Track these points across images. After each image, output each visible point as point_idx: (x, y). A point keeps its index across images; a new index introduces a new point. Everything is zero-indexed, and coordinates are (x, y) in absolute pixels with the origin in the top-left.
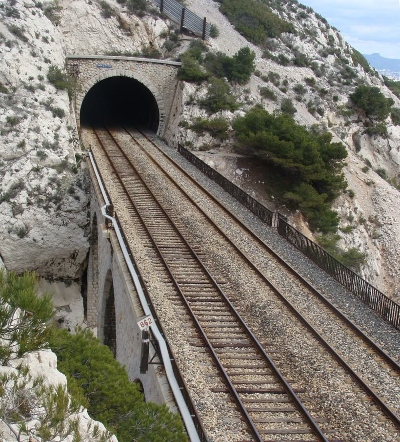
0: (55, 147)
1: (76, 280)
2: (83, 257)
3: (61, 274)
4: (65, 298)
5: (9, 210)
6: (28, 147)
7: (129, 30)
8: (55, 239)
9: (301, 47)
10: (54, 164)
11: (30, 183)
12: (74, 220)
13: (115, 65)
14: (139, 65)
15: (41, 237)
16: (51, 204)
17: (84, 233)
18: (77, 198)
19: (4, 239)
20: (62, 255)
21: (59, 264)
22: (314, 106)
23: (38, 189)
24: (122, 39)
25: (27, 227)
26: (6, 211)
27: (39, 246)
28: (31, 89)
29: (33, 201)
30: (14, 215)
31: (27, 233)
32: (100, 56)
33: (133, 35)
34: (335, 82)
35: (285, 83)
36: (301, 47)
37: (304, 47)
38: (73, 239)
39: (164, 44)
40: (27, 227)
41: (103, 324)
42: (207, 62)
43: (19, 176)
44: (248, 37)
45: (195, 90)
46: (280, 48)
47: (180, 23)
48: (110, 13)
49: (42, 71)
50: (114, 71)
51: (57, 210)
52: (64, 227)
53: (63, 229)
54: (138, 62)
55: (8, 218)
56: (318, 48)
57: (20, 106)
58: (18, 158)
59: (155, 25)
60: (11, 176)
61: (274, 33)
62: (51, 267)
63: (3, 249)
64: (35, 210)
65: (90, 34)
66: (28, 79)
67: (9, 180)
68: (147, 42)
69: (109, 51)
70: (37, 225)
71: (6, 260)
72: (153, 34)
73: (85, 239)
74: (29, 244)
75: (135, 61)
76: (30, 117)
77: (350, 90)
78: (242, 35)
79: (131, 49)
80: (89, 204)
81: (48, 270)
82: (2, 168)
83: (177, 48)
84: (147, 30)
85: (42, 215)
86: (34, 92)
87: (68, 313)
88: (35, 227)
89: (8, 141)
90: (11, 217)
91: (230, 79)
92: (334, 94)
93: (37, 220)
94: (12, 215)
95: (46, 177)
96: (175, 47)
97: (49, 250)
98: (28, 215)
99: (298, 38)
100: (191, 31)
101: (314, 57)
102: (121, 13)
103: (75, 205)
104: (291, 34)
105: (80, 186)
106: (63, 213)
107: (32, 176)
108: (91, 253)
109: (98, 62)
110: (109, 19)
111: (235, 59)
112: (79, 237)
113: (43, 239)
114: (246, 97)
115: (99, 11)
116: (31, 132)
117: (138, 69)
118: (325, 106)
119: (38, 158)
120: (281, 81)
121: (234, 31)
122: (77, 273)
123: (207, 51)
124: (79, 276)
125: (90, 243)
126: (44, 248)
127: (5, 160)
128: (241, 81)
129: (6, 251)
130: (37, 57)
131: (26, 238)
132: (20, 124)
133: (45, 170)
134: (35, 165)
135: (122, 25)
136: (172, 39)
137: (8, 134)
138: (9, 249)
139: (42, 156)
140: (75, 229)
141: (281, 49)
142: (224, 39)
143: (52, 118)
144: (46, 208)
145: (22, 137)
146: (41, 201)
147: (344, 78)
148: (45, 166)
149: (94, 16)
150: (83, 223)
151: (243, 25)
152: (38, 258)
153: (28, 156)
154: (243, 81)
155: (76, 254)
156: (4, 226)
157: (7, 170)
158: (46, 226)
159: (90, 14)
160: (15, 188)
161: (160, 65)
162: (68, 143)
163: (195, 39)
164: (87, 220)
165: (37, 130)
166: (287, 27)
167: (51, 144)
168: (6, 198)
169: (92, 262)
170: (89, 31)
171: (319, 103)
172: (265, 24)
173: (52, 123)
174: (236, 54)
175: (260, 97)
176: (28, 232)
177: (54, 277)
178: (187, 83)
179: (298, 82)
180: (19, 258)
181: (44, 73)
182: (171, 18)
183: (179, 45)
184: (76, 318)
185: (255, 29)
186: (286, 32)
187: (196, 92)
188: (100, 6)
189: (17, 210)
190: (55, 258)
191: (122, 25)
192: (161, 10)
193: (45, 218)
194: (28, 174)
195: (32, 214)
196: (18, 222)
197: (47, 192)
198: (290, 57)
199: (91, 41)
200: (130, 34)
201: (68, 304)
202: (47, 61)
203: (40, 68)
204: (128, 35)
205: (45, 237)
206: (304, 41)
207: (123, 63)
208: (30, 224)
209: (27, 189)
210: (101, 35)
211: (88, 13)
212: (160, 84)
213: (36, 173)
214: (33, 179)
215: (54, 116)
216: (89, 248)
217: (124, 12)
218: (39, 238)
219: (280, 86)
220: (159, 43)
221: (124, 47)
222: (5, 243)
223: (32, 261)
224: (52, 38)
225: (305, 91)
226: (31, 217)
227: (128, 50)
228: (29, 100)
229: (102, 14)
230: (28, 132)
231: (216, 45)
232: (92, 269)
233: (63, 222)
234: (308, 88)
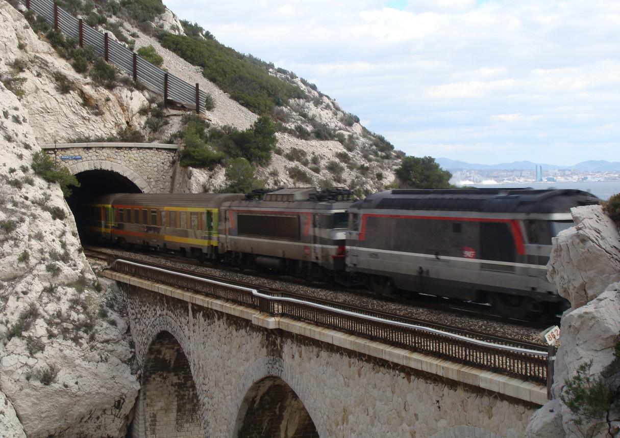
0: (65, 258)
2: (131, 404)
5: (23, 348)
6: (33, 261)
7: (97, 107)
8: (94, 382)
9: (318, 115)
10: (70, 281)
11: (46, 309)
12: (114, 353)
13: (86, 155)
17: (130, 370)
19: (21, 390)
20: (103, 404)
21: (98, 418)
22: (358, 187)
23: (59, 314)
24: (89, 120)
25: (52, 369)
26: (19, 350)
27: (73, 394)
28: (17, 184)
29: (56, 332)
30: (32, 354)
31: (54, 378)
32: (62, 144)
33: (104, 113)
34: (372, 156)
36: (318, 115)
37: (322, 115)
39: (147, 123)
40: (52, 369)
42: (213, 140)
43: (29, 300)
44: (251, 106)
45: (208, 178)
46: (293, 118)
48: (69, 87)
50: (86, 163)
52: (103, 364)
53: (103, 367)
54: (118, 148)
55: (24, 359)
56: (338, 115)
57: (10, 206)
58: (22, 277)
59: (131, 99)
60: (17, 301)
61: (282, 100)
62: (85, 425)
63: (21, 405)
65: (44, 117)
66: (7, 171)
67: (15, 308)
68: (124, 121)
70: (67, 365)
71: (25, 421)
72: (130, 111)
74: (57, 392)
75: (113, 147)
76: (27, 219)
77: (394, 165)
78: (242, 104)
79: (103, 133)
80: (129, 330)
81: (82, 430)
82: (2, 291)
83: (164, 127)
84: (121, 105)
85: (71, 350)
86: (20, 188)
88: (64, 369)
89: (6, 254)
90: (29, 357)
92: (376, 171)
93: (65, 357)
95: (64, 299)
96: (161, 126)
97: (87, 399)
98: (52, 352)
99: (311, 105)
100: (180, 103)
101: (336, 126)
102: (83, 86)
103: (113, 333)
105: (111, 307)
106: (99, 345)
107: (45, 300)
108: (141, 398)
109: (63, 152)
110: (68, 95)
111: (252, 132)
112: (125, 375)
113: (77, 383)
114: (275, 181)
115: (52, 85)
117: (119, 158)
120: (309, 158)
121: (230, 100)
123: (208, 127)
125: (140, 382)
126: (79, 396)
127: (4, 280)
128: (262, 161)
130: (14, 141)
131: (53, 385)
132: (18, 230)
133: (60, 289)
134: (47, 284)
135: (87, 101)
136: (156, 115)
137: (3, 244)
138: (30, 404)
139: (54, 271)
140: (118, 365)
141: (294, 119)
143: (52, 221)
144: (76, 340)
145: (22, 247)
146: (65, 331)
147: (382, 150)
148: (59, 285)
149: (47, 92)
150: (126, 356)
152: (71, 412)
153: (35, 272)
154: (264, 161)
155: (122, 401)
156: (20, 371)
157: (11, 294)
159: (41, 90)
160: (26, 318)
161: (148, 151)
162: (78, 252)
164: (131, 352)
165: (39, 237)
166: (295, 91)
167: (60, 255)
168: (16, 332)
171: (364, 183)
172: (268, 88)
173: (54, 228)
174: (251, 126)
175: (291, 180)
176: (56, 375)
178: (194, 169)
179: (329, 159)
180: (43, 415)
181: (27, 162)
183: (166, 123)
185: (257, 96)
186: (294, 98)
187: (209, 180)
189: (35, 347)
191: (87, 101)
192: (135, 78)
194: (40, 297)
195: (57, 349)
196: (40, 363)
197: (71, 318)
198: (309, 128)
200: (99, 113)
202: (27, 147)
203: (20, 157)
204: (96, 114)
205: (79, 380)
206: (320, 107)
207: (98, 151)
208: (56, 365)
209: (43, 317)
210: (60, 117)
211: (37, 89)
212: (150, 176)
213: (50, 295)
214: (47, 303)
215: (54, 218)
216: (139, 391)
217: (88, 84)
218: (71, 383)
220: (139, 122)
221: (93, 130)
222: (23, 395)
224: (24, 117)
225: (342, 169)
227: (99, 135)
228: (18, 199)
231: (215, 119)
232: (143, 422)
233: (101, 357)
234: (343, 165)
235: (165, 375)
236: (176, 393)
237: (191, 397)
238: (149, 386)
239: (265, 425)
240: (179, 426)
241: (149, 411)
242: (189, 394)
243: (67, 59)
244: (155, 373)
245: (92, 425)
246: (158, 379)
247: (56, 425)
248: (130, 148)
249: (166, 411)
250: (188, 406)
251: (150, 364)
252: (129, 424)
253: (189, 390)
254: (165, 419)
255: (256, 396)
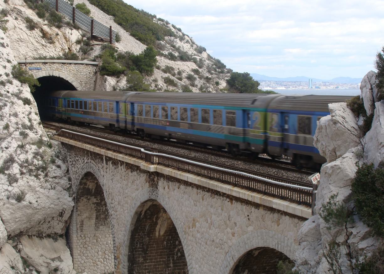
0: (31, 128)
1: (61, 236)
3: (49, 232)
4: (55, 251)
6: (11, 129)
7: (51, 39)
8: (47, 201)
9: (182, 47)
10: (33, 142)
12: (59, 184)
13: (44, 67)
14: (64, 66)
15: (36, 200)
16: (40, 172)
18: (59, 167)
21: (49, 222)
22: (204, 90)
23: (27, 161)
24: (46, 46)
27: (34, 208)
29: (25, 171)
30: (10, 184)
31: (23, 198)
32: (29, 60)
33: (55, 43)
34: (213, 72)
35: (179, 73)
37: (184, 46)
38: (61, 200)
39: (80, 49)
40: (23, 193)
41: (127, 253)
44: (143, 40)
47: (90, 32)
49: (7, 70)
50: (44, 72)
51: (45, 177)
52: (53, 191)
53: (52, 192)
54: (63, 63)
55: (6, 187)
58: (5, 139)
60: (2, 152)
63: (4, 213)
64: (27, 178)
65: (19, 44)
68: (67, 48)
69: (38, 57)
70: (31, 191)
72: (70, 42)
73: (70, 199)
74: (25, 206)
76: (9, 105)
77: (225, 77)
78: (137, 39)
80: (68, 171)
81: (39, 229)
83: (91, 52)
84: (65, 38)
85: (34, 182)
86: (4, 86)
87: (60, 263)
88: (29, 193)
90: (9, 186)
91: (141, 72)
92: (215, 81)
93: (30, 186)
94: (9, 184)
95: (30, 152)
96: (89, 51)
97: (43, 211)
98: (22, 183)
99: (178, 40)
100: (100, 38)
101: (192, 53)
103: (59, 173)
104: (172, 37)
105: (58, 157)
106: (50, 179)
107: (19, 152)
108: (75, 211)
109: (30, 65)
110: (34, 31)
112: (66, 197)
113: (37, 201)
114: (156, 85)
115: (24, 25)
116: (11, 117)
117: (63, 69)
118: (212, 89)
119: (21, 137)
120: (176, 72)
122: (62, 229)
124: (64, 232)
125: (74, 202)
126: (38, 209)
128: (148, 73)
129: (6, 215)
131: (23, 202)
132: (3, 111)
133: (27, 146)
134: (20, 143)
135: (45, 35)
136: (86, 44)
138: (9, 213)
139: (24, 135)
142: (125, 43)
143: (23, 105)
144: (37, 176)
146: (31, 171)
149: (21, 29)
150: (66, 186)
151: (137, 32)
153: (13, 136)
155: (63, 212)
156: (3, 194)
158: (39, 191)
160: (7, 162)
161: (81, 65)
162: (38, 125)
163: (105, 43)
164: (69, 184)
165: (16, 115)
167: (28, 126)
169: (76, 218)
170: (18, 41)
171: (208, 87)
172: (153, 30)
174: (142, 52)
175: (165, 85)
176: (25, 197)
177: (44, 235)
178: (108, 77)
179: (188, 73)
180: (17, 220)
181: (9, 70)
182: (82, 28)
183: (92, 49)
184: (68, 266)
185: (146, 35)
186: (168, 36)
187: (117, 83)
188: (25, 21)
189: (12, 180)
190: (47, 217)
191: (45, 35)
192: (74, 22)
193: (37, 185)
194: (16, 151)
196: (15, 189)
197: (34, 163)
198: (176, 54)
199: (20, 50)
200: (52, 43)
201: (59, 255)
204: (50, 43)
205: (38, 200)
206: (183, 42)
207: (51, 65)
208: (25, 190)
211: (15, 27)
212: (82, 80)
214: (20, 154)
216: (74, 207)
217: (45, 25)
218: (34, 201)
219: (176, 76)
220: (76, 48)
221: (48, 52)
223: (28, 222)
224: (7, 44)
225: (195, 79)
226: (25, 184)
227: (52, 55)
229: (27, 27)
230: (9, 117)
232: (76, 225)
234: (196, 76)
235: (89, 198)
236: (95, 208)
237: (104, 210)
238: (79, 204)
239: (147, 227)
240: (97, 227)
241: (79, 218)
242: (103, 209)
243: (33, 10)
244: (83, 197)
245: (45, 226)
246: (85, 200)
247: (24, 226)
248: (70, 64)
249: (89, 218)
250: (102, 216)
251: (80, 191)
252: (67, 226)
253: (103, 207)
254: (89, 223)
255: (142, 211)
